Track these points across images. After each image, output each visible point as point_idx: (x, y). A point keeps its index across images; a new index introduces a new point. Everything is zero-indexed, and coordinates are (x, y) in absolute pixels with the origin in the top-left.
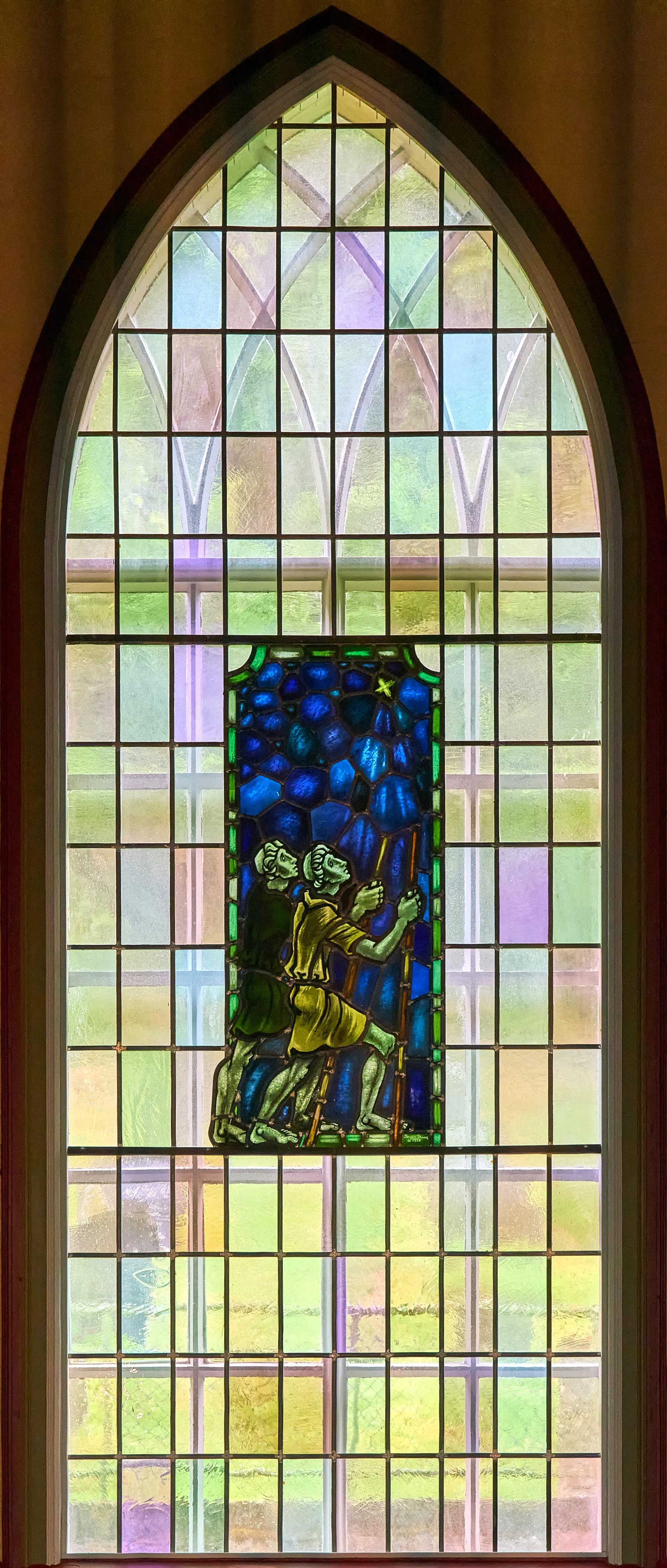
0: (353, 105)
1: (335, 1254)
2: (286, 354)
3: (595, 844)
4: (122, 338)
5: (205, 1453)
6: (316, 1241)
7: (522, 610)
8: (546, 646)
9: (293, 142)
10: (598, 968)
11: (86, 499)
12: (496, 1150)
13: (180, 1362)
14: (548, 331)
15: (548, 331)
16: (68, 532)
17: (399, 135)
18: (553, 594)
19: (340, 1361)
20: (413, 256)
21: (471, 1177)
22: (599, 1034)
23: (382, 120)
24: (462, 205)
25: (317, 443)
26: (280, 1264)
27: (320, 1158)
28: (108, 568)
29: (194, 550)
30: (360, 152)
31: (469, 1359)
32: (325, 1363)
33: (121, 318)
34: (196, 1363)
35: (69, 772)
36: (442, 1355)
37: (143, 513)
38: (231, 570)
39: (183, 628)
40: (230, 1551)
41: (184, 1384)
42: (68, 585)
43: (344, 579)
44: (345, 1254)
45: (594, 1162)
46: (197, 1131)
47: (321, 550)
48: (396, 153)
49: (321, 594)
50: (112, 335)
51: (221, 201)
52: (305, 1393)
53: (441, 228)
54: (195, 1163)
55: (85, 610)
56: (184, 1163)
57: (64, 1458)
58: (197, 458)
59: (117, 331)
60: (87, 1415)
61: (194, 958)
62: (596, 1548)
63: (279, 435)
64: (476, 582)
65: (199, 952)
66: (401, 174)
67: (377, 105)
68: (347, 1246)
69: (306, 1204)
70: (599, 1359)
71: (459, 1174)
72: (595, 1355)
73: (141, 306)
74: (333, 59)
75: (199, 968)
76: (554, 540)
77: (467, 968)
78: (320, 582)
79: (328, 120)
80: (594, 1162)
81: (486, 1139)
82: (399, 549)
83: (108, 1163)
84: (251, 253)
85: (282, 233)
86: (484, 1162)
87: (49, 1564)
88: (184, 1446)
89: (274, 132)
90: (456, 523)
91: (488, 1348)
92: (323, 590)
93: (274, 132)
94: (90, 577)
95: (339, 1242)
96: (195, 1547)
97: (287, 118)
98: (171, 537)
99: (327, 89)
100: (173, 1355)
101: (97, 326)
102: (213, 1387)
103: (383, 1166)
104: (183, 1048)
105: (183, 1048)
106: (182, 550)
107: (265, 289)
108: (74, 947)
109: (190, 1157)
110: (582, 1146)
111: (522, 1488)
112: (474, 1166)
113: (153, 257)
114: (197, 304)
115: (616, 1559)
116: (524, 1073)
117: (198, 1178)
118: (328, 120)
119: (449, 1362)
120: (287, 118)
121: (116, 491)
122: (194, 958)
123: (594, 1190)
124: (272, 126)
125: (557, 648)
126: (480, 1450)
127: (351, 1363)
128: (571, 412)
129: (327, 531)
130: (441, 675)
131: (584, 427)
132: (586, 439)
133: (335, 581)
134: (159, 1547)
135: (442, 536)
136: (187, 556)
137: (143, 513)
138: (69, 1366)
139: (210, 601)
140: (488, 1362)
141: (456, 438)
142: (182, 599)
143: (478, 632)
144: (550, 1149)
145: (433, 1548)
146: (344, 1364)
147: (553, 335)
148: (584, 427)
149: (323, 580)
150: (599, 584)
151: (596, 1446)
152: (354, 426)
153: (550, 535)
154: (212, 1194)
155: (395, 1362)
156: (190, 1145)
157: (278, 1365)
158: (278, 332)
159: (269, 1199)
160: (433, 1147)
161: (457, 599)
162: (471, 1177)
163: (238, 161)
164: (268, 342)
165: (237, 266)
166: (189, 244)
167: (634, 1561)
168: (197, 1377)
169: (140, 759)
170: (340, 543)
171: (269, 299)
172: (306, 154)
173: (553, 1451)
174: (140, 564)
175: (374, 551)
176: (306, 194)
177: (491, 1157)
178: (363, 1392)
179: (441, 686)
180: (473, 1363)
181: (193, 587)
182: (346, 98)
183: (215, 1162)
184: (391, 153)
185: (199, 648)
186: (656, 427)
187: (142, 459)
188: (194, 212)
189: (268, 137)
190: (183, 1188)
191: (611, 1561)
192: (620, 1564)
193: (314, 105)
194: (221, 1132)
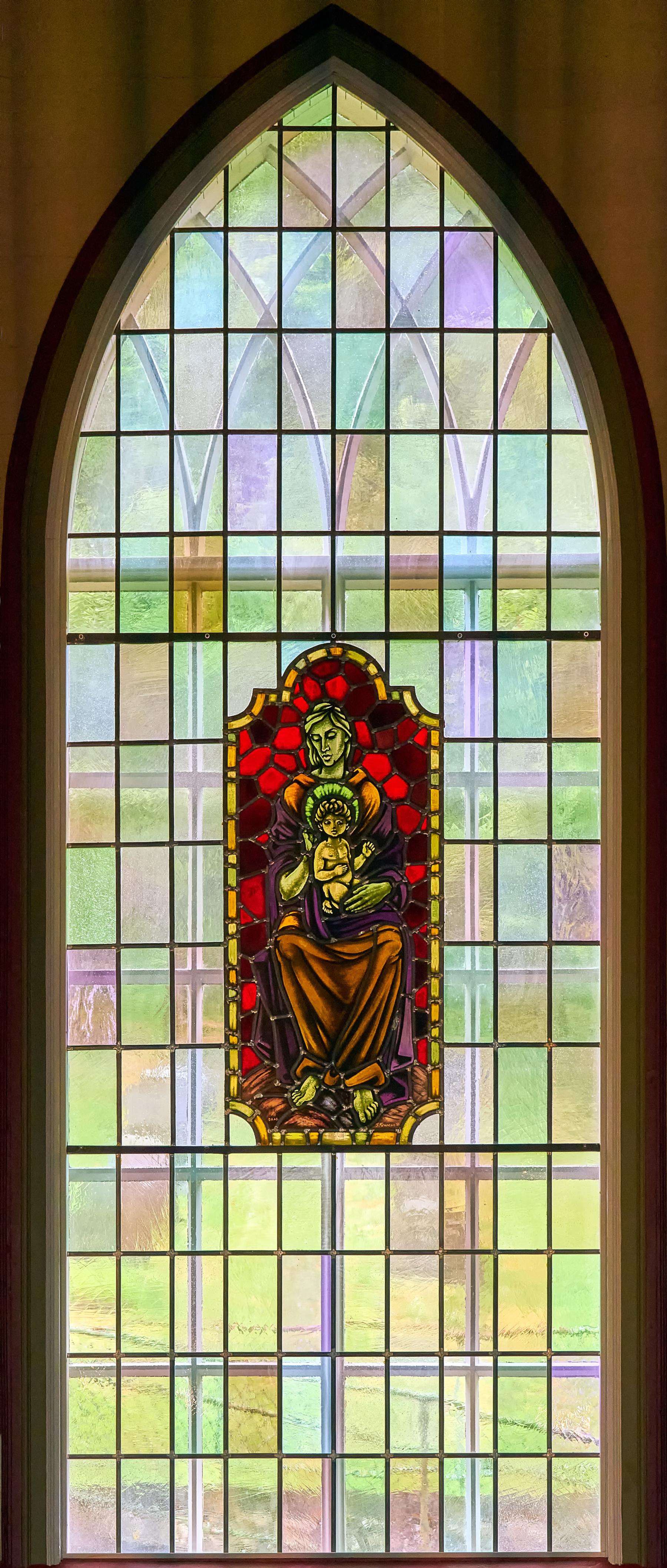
0: (354, 108)
1: (332, 1254)
3: (595, 740)
6: (315, 1341)
7: (522, 610)
9: (295, 145)
10: (597, 966)
12: (496, 1148)
14: (549, 331)
15: (549, 331)
17: (399, 137)
18: (553, 591)
19: (338, 1359)
20: (414, 257)
22: (597, 925)
23: (381, 121)
24: (462, 207)
25: (317, 438)
27: (318, 1156)
29: (194, 547)
30: (360, 160)
33: (123, 318)
34: (194, 1362)
36: (441, 1354)
39: (183, 625)
42: (70, 585)
48: (397, 154)
51: (222, 203)
52: (304, 1395)
53: (442, 229)
54: (193, 1162)
58: (199, 457)
59: (119, 332)
60: (85, 1409)
61: (195, 752)
62: (596, 1548)
63: (280, 229)
67: (379, 106)
68: (345, 1346)
69: (306, 1198)
71: (460, 1173)
72: (595, 1353)
73: (143, 306)
74: (334, 57)
75: (200, 769)
77: (467, 966)
78: (319, 582)
80: (593, 1159)
81: (484, 625)
84: (254, 256)
86: (484, 1160)
87: (49, 1564)
88: (183, 1446)
89: (276, 134)
90: (456, 520)
91: (488, 1346)
93: (276, 134)
94: (90, 578)
96: (194, 1547)
97: (288, 120)
98: (172, 534)
101: (100, 323)
102: (211, 1385)
104: (181, 843)
105: (181, 843)
106: (183, 547)
107: (268, 291)
108: (74, 845)
109: (189, 1155)
110: (582, 1145)
111: (523, 1480)
114: (197, 304)
115: (616, 1558)
116: (523, 1069)
117: (196, 1177)
119: (448, 1361)
120: (288, 120)
122: (195, 752)
124: (273, 129)
126: (480, 1246)
127: (349, 1361)
128: (569, 411)
129: (327, 528)
130: (440, 717)
131: (585, 428)
133: (334, 583)
135: (441, 533)
136: (187, 553)
138: (68, 1366)
139: (209, 600)
140: (488, 1361)
142: (183, 597)
143: (478, 629)
144: (550, 1148)
145: (217, 1548)
146: (342, 1362)
147: (554, 335)
148: (584, 427)
150: (598, 581)
151: (596, 731)
152: (355, 425)
153: (549, 534)
154: (211, 1189)
155: (394, 1362)
156: (189, 1144)
157: (275, 1365)
159: (268, 1200)
161: (456, 598)
163: (233, 164)
164: (269, 340)
167: (634, 1560)
168: (195, 1375)
169: (139, 868)
171: (271, 302)
172: (309, 157)
173: (552, 1449)
176: (308, 192)
177: (490, 1155)
181: (472, 584)
182: (347, 100)
186: (655, 424)
190: (183, 1189)
191: (612, 1561)
192: (620, 1563)
193: (313, 108)
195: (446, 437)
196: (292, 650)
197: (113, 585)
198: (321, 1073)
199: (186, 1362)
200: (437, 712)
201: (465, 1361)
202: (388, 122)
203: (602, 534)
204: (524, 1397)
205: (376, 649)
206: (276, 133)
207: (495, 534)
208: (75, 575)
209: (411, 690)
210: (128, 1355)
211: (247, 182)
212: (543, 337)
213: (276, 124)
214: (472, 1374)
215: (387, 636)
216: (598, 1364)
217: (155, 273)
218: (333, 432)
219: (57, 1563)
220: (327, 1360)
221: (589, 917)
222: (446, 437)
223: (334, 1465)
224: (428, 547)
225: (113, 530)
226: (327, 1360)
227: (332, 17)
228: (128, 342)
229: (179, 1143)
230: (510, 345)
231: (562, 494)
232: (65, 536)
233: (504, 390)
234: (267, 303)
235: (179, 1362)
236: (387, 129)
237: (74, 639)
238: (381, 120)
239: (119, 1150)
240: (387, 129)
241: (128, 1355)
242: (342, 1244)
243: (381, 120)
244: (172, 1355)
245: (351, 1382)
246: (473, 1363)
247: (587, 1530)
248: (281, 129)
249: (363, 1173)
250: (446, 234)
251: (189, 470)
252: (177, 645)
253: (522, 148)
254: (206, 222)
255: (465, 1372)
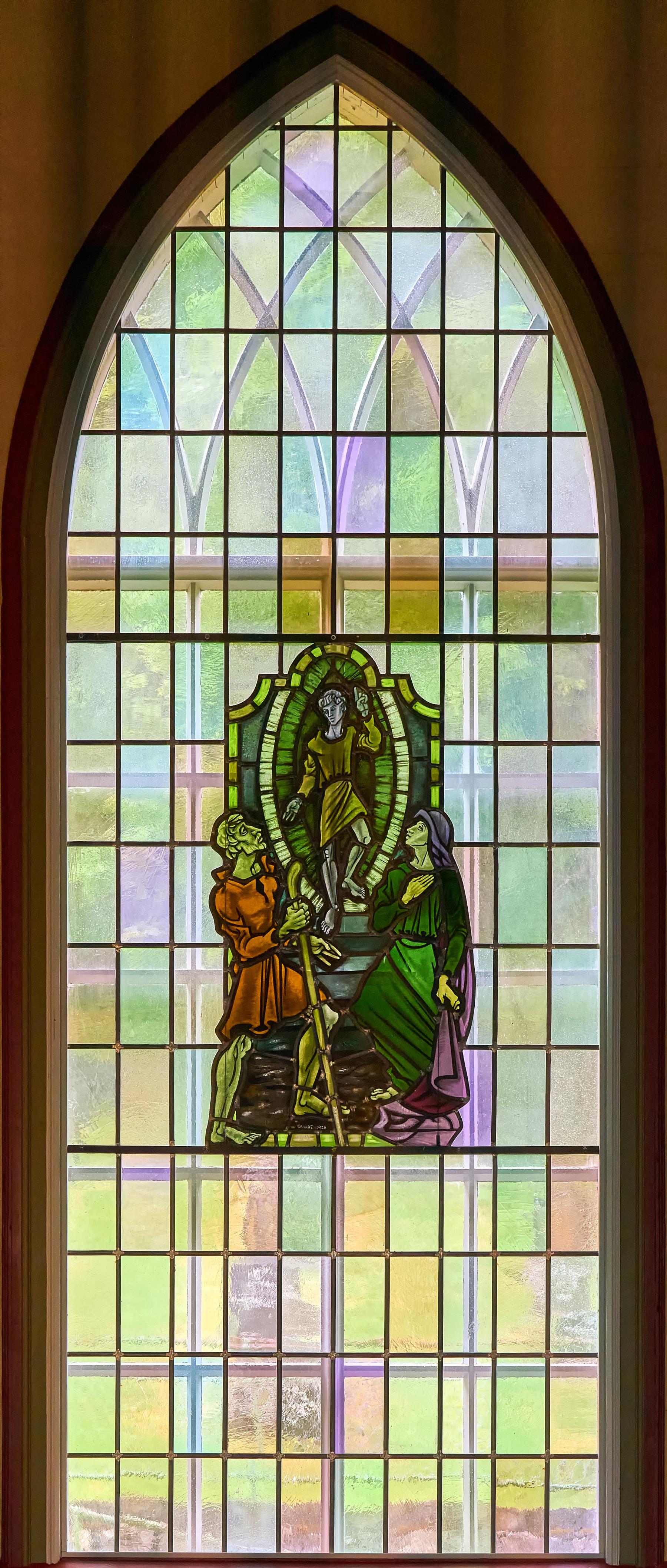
0: (358, 108)
2: (288, 355)
4: (126, 337)
5: (204, 1452)
8: (546, 645)
9: (296, 143)
10: (597, 967)
11: (88, 500)
13: (179, 1361)
14: (549, 333)
15: (549, 333)
16: (70, 529)
17: (401, 138)
20: (416, 253)
21: (471, 1176)
23: (383, 121)
24: (463, 206)
26: (118, 1263)
28: (594, 568)
30: (362, 154)
31: (467, 1359)
32: (322, 1362)
33: (123, 317)
35: (70, 770)
37: (145, 511)
38: (125, 569)
39: (182, 627)
40: (228, 1551)
41: (182, 1385)
42: (70, 584)
43: (344, 579)
44: (344, 1254)
45: (593, 1162)
46: (192, 1129)
47: (268, 549)
49: (320, 594)
50: (115, 335)
53: (443, 230)
55: (84, 608)
56: (183, 1161)
57: (602, 1456)
59: (120, 331)
60: (85, 1407)
62: (594, 1548)
64: (475, 583)
65: (199, 950)
66: (403, 175)
67: (380, 106)
70: (596, 1360)
74: (338, 58)
75: (199, 770)
76: (230, 540)
79: (330, 121)
80: (593, 1162)
82: (291, 549)
83: (108, 1161)
84: (256, 254)
85: (285, 234)
87: (48, 1562)
88: (182, 1445)
90: (458, 522)
92: (323, 591)
94: (91, 574)
95: (338, 1242)
99: (330, 89)
100: (172, 1354)
102: (211, 1387)
103: (168, 1166)
104: (485, 1047)
107: (269, 293)
112: (194, 1164)
113: (155, 257)
117: (196, 1176)
118: (330, 121)
121: (114, 490)
123: (592, 1190)
124: (275, 128)
125: (556, 647)
127: (349, 1362)
128: (570, 412)
130: (441, 707)
131: (583, 429)
132: (585, 441)
134: (318, 1547)
137: (145, 511)
140: (487, 1362)
141: (458, 438)
142: (182, 598)
145: (215, 1548)
146: (342, 1363)
147: (554, 337)
149: (322, 579)
155: (125, 1361)
158: (281, 332)
160: (349, 1147)
162: (471, 1176)
163: (237, 164)
164: (268, 343)
165: (240, 267)
166: (193, 244)
167: (632, 1562)
170: (340, 542)
171: (272, 302)
172: (309, 160)
173: (550, 1441)
174: (575, 562)
175: (427, 550)
176: (309, 196)
178: (360, 1393)
179: (441, 722)
180: (194, 1363)
183: (216, 1161)
184: (394, 156)
185: (198, 646)
187: (145, 458)
188: (196, 213)
189: (269, 139)
190: (183, 1186)
192: (616, 1564)
193: (317, 107)
194: (219, 1131)
195: (448, 440)
196: (292, 651)
197: (113, 583)
198: (319, 1091)
199: (186, 1361)
200: (437, 702)
201: (464, 1362)
202: (390, 122)
203: (601, 536)
204: (522, 1395)
205: (377, 652)
206: (278, 132)
207: (495, 536)
208: (75, 573)
209: (407, 677)
210: (127, 1354)
211: (250, 188)
212: (542, 340)
213: (278, 124)
214: (471, 1375)
215: (388, 638)
216: (597, 1365)
217: (156, 271)
218: (334, 434)
219: (55, 1562)
220: (327, 1361)
221: (402, 626)
222: (448, 440)
223: (332, 1465)
224: (159, 548)
225: (167, 529)
226: (327, 1361)
227: (334, 17)
228: (126, 338)
229: (178, 1143)
230: (510, 346)
231: (559, 494)
232: (64, 534)
233: (504, 392)
234: (267, 304)
235: (179, 1361)
236: (389, 129)
237: (75, 638)
238: (382, 120)
239: (118, 1150)
240: (389, 129)
241: (127, 1354)
242: (343, 1244)
243: (382, 120)
244: (172, 1354)
245: (350, 1382)
246: (471, 1363)
247: (580, 1505)
248: (283, 128)
249: (361, 1175)
250: (448, 235)
251: (187, 467)
252: (178, 645)
253: (523, 151)
254: (208, 222)
255: (463, 1373)
